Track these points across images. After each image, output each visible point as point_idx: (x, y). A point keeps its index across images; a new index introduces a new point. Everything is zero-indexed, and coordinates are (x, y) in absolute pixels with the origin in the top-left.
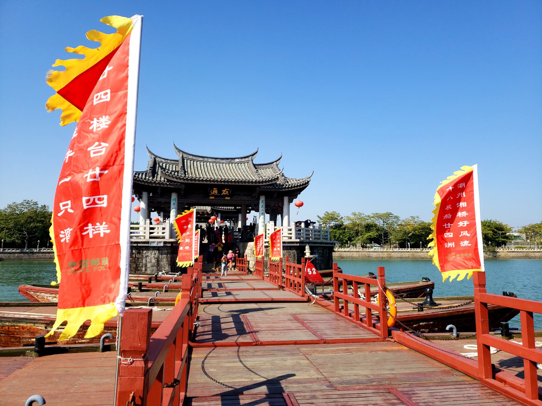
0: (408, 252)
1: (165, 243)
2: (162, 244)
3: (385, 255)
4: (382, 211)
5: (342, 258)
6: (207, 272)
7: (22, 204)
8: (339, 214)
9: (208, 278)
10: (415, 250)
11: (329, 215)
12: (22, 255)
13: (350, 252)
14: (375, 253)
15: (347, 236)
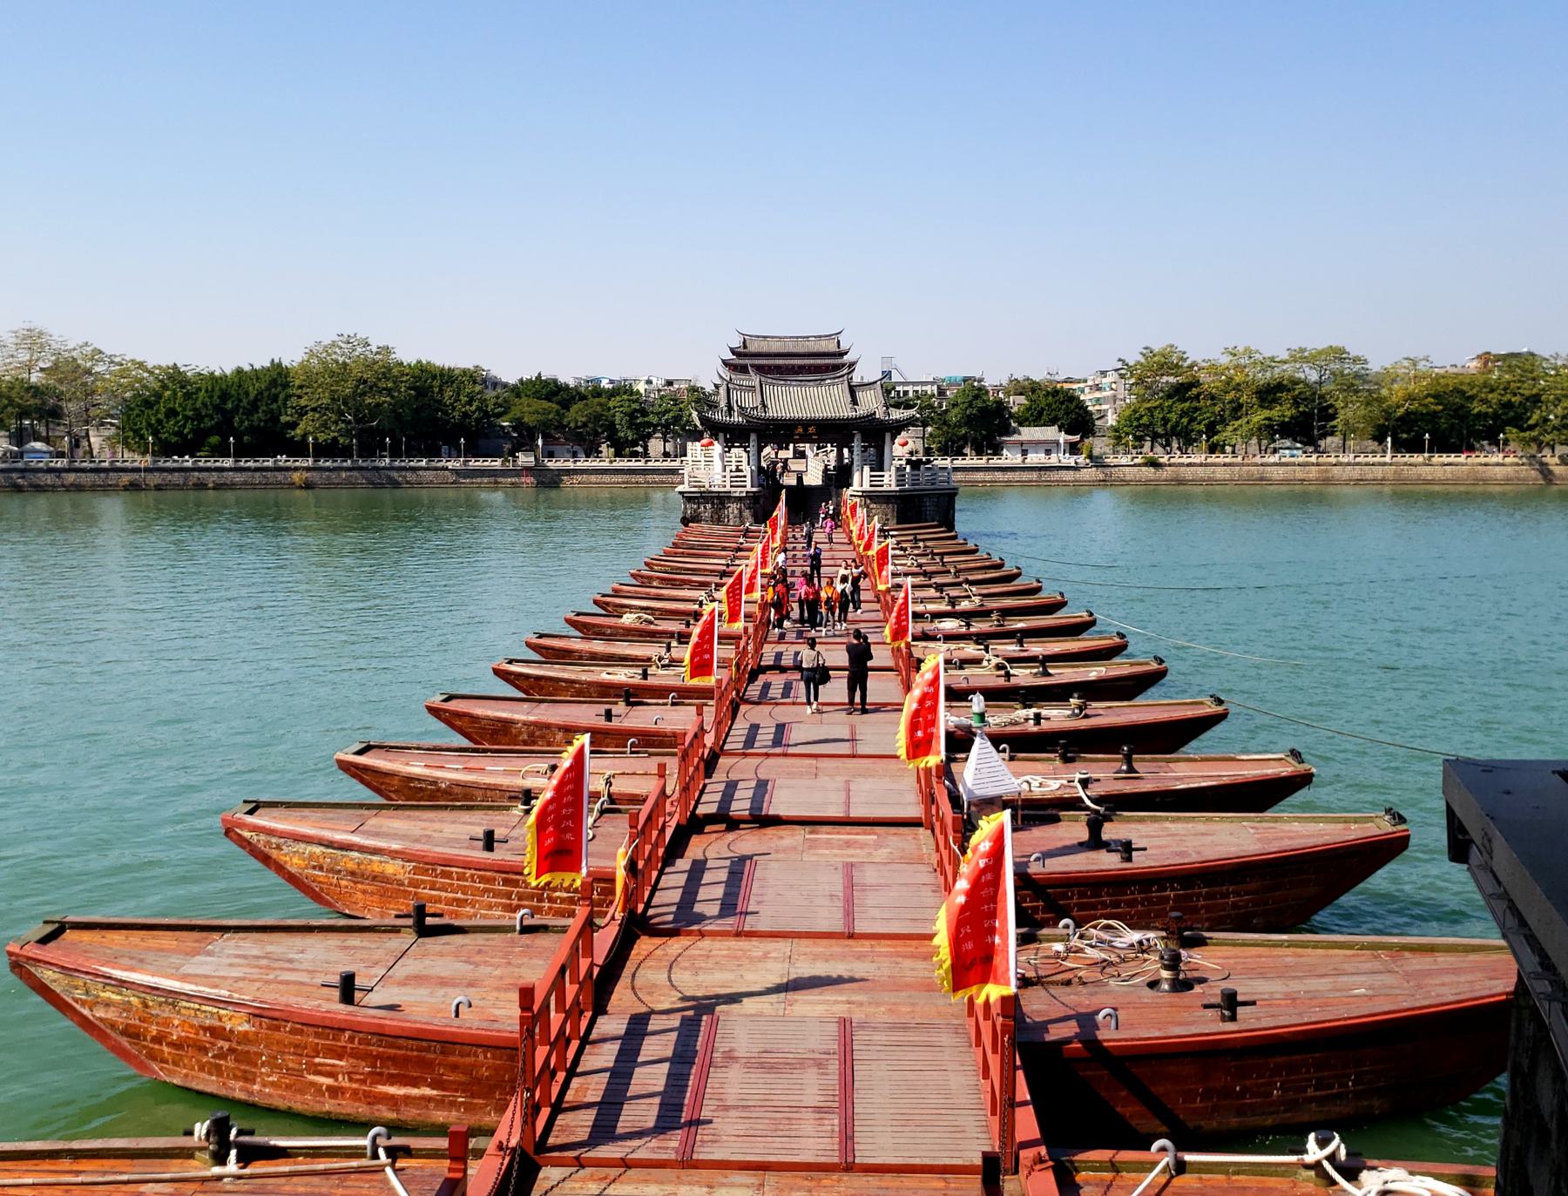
0: (1385, 464)
1: (747, 492)
2: (744, 494)
3: (1313, 472)
4: (1316, 341)
5: (1180, 482)
6: (793, 524)
7: (334, 344)
8: (1184, 353)
9: (794, 531)
10: (1407, 458)
11: (1154, 356)
12: (355, 473)
13: (1206, 465)
14: (1282, 470)
15: (1204, 419)
